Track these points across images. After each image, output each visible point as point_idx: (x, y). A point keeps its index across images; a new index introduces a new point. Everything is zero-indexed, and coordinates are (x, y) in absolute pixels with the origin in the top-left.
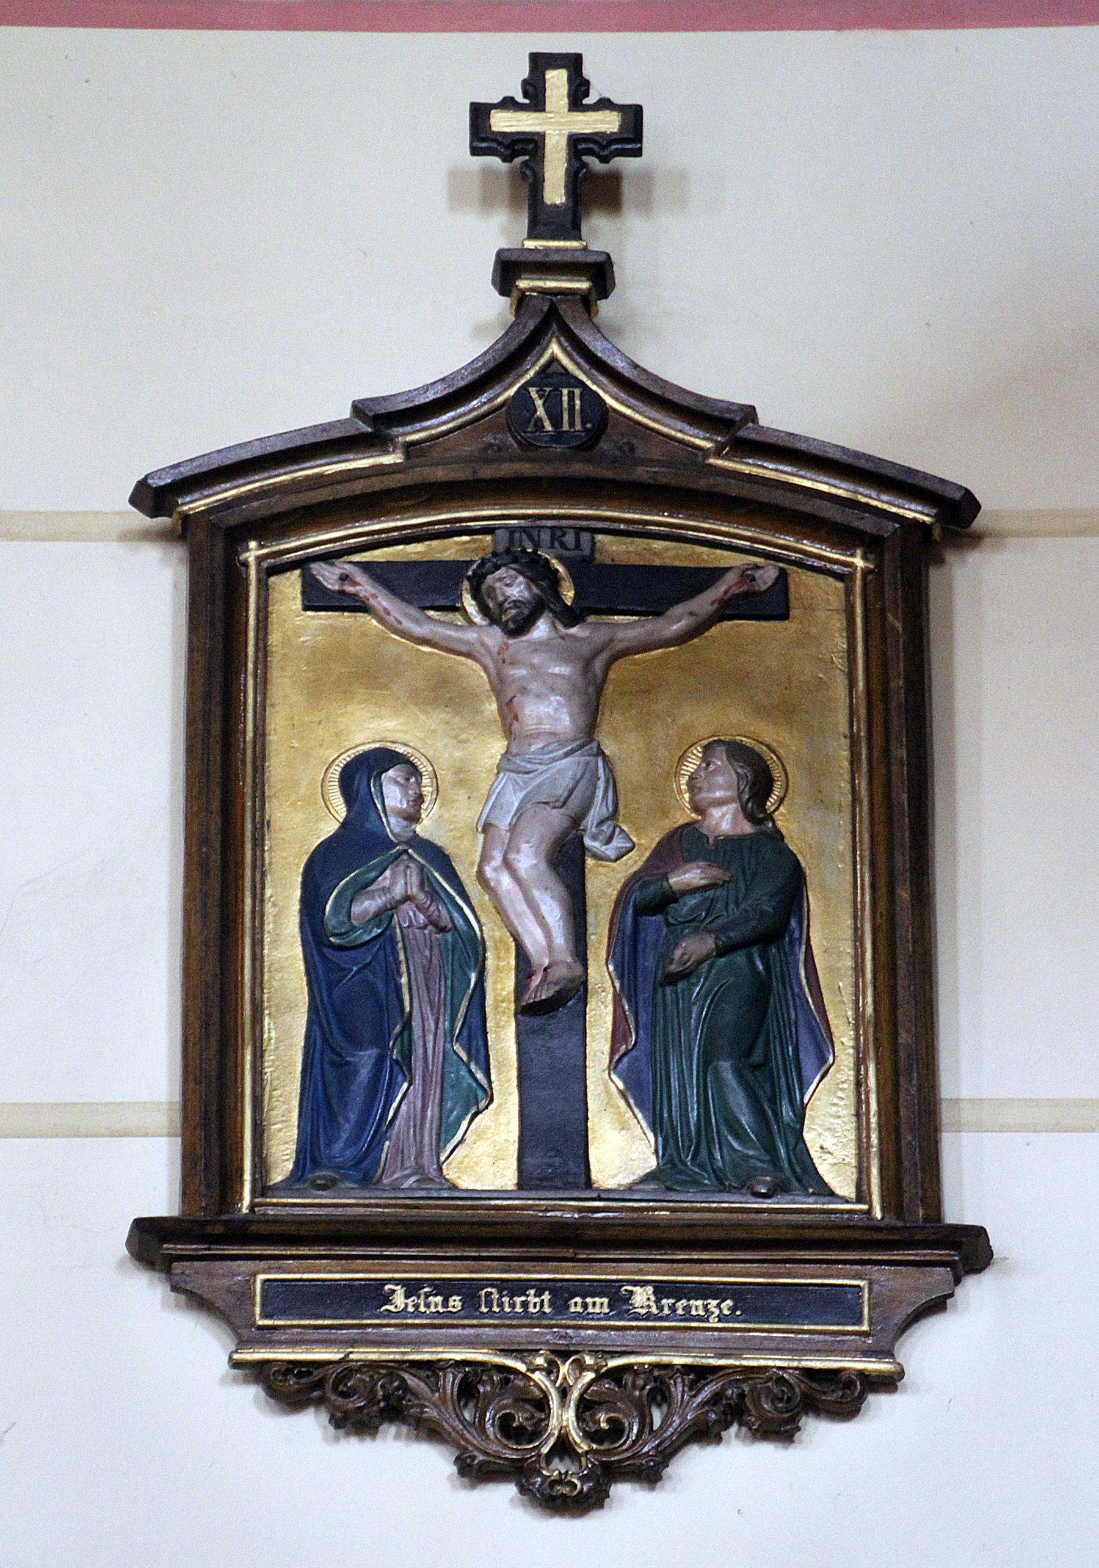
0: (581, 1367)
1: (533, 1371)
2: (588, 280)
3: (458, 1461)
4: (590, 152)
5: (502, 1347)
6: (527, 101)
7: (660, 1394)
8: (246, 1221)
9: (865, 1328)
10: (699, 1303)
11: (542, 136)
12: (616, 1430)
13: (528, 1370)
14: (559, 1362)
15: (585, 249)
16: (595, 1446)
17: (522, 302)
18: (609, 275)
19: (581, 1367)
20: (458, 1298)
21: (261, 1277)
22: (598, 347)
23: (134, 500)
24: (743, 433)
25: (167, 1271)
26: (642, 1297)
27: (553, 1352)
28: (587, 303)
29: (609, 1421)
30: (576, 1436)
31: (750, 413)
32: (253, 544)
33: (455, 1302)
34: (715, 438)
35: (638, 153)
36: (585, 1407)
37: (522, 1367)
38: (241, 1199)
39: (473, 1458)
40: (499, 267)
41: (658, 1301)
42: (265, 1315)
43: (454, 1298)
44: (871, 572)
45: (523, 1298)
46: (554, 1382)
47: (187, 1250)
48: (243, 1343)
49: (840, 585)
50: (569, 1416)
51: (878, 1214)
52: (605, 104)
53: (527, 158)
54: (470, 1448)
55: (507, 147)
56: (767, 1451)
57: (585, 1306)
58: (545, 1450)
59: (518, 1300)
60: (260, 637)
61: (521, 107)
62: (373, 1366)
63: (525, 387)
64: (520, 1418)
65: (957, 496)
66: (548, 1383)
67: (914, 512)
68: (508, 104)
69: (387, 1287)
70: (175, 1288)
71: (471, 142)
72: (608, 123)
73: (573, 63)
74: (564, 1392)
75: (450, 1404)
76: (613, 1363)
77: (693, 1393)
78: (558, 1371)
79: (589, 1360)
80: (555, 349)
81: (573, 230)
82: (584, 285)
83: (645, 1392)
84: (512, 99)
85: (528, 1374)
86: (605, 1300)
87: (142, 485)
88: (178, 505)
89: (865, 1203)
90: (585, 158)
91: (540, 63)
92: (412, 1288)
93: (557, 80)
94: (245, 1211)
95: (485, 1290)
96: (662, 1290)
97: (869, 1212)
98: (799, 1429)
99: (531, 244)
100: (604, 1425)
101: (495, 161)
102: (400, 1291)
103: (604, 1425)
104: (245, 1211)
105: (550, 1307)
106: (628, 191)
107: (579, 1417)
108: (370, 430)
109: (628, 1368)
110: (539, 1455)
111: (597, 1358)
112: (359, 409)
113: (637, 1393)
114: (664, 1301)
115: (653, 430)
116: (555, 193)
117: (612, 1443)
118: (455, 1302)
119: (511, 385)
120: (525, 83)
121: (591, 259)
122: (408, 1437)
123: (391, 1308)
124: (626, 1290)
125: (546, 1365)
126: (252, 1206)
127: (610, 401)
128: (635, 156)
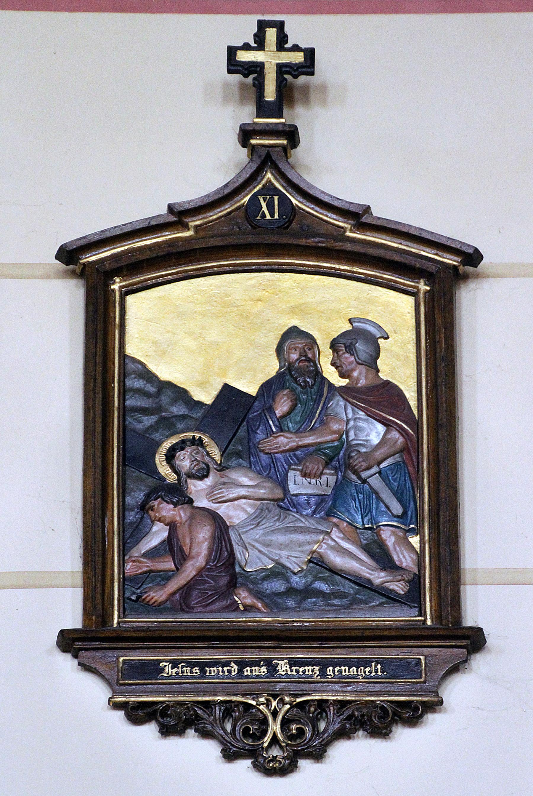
0: (282, 702)
2: (286, 139)
3: (223, 751)
8: (114, 630)
10: (215, 668)
12: (301, 732)
13: (257, 704)
17: (253, 150)
19: (282, 702)
20: (197, 668)
21: (121, 659)
22: (291, 175)
23: (57, 257)
25: (75, 656)
26: (283, 667)
27: (269, 695)
29: (297, 729)
30: (280, 736)
31: (367, 209)
32: (118, 280)
33: (196, 670)
34: (349, 221)
35: (312, 74)
36: (285, 723)
37: (254, 703)
38: (113, 619)
40: (241, 134)
41: (290, 668)
44: (428, 292)
45: (228, 668)
47: (350, 644)
48: (115, 693)
49: (410, 300)
51: (429, 622)
52: (296, 48)
55: (246, 69)
57: (251, 671)
58: (266, 745)
59: (225, 669)
60: (420, 407)
63: (255, 196)
64: (252, 728)
65: (471, 251)
66: (266, 711)
67: (450, 260)
68: (246, 47)
70: (80, 664)
71: (228, 67)
72: (298, 58)
74: (275, 714)
75: (218, 722)
76: (298, 700)
77: (338, 715)
78: (271, 704)
79: (287, 699)
80: (269, 175)
82: (285, 142)
85: (258, 707)
88: (80, 259)
89: (420, 615)
90: (286, 76)
91: (262, 26)
92: (175, 664)
93: (271, 34)
94: (115, 625)
95: (181, 664)
96: (293, 662)
99: (256, 120)
100: (294, 731)
101: (237, 78)
103: (294, 731)
104: (115, 625)
106: (313, 95)
108: (175, 219)
109: (307, 701)
110: (262, 748)
111: (291, 698)
112: (171, 208)
113: (311, 715)
114: (293, 668)
115: (310, 213)
118: (196, 670)
119: (247, 195)
120: (255, 35)
122: (198, 737)
123: (165, 675)
125: (265, 702)
126: (118, 623)
127: (294, 201)
128: (311, 75)
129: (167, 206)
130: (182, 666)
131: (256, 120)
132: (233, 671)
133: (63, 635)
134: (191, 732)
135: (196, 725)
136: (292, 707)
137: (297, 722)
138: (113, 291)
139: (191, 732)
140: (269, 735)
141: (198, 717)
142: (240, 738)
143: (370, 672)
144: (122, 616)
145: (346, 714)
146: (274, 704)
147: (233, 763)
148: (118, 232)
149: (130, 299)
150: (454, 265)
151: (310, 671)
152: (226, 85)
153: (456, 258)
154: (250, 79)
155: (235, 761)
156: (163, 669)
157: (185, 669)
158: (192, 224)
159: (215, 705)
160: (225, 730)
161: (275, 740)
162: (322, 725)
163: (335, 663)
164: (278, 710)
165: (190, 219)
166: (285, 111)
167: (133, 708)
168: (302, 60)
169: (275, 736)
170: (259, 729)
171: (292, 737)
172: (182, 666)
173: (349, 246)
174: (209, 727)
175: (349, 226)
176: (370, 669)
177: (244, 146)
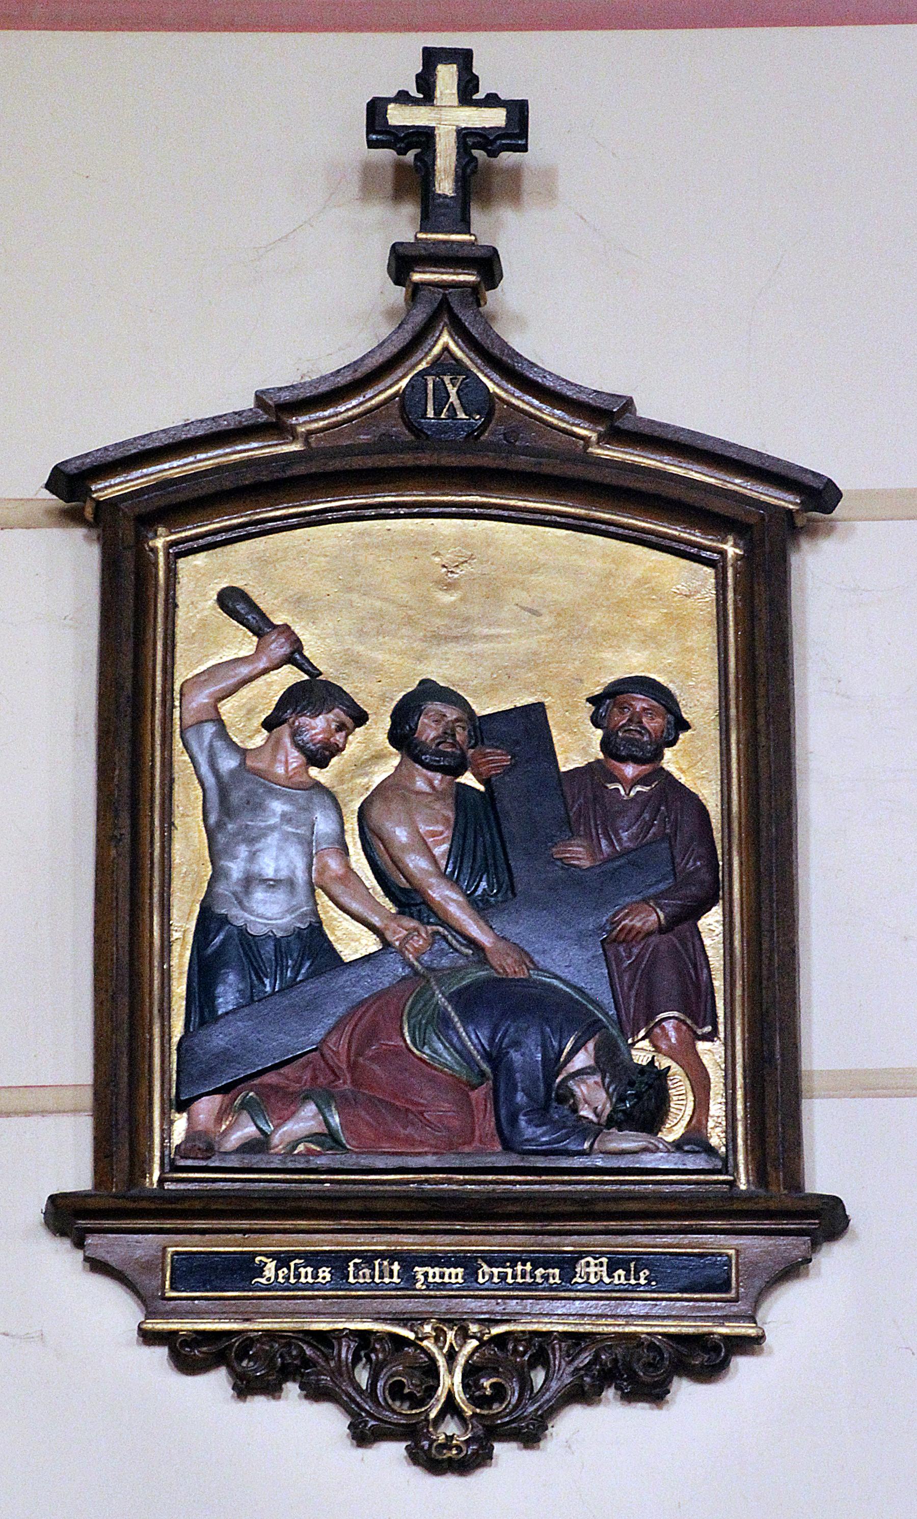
0: (464, 1335)
1: (422, 1340)
2: (479, 274)
4: (476, 146)
5: (377, 1316)
6: (421, 96)
7: (541, 1358)
9: (733, 1294)
11: (433, 128)
12: (499, 1392)
13: (417, 1338)
14: (445, 1329)
15: (472, 244)
16: (478, 1411)
17: (416, 290)
18: (495, 268)
19: (464, 1335)
20: (328, 1270)
24: (625, 424)
25: (79, 1244)
28: (475, 295)
30: (460, 1397)
32: (161, 530)
33: (325, 1274)
35: (524, 148)
36: (471, 1373)
37: (412, 1336)
39: (366, 1422)
42: (173, 1288)
43: (324, 1269)
46: (441, 1348)
48: (150, 1315)
49: (710, 571)
50: (445, 1380)
52: (492, 101)
53: (419, 150)
54: (363, 1414)
56: (641, 1411)
58: (432, 1415)
61: (416, 102)
62: (270, 1335)
65: (817, 484)
67: (788, 501)
68: (403, 98)
69: (258, 1259)
70: (87, 1259)
72: (496, 118)
73: (464, 58)
74: (451, 1357)
80: (445, 338)
81: (465, 225)
83: (526, 1358)
84: (407, 92)
86: (557, 1271)
87: (57, 471)
91: (431, 57)
92: (283, 1260)
97: (732, 1184)
98: (669, 1392)
99: (420, 236)
100: (488, 1392)
101: (386, 155)
102: (271, 1265)
105: (399, 1277)
106: (528, 183)
107: (466, 1386)
112: (260, 398)
116: (445, 185)
117: (501, 1403)
118: (325, 1274)
120: (418, 76)
121: (478, 254)
123: (263, 1281)
124: (261, 1261)
126: (161, 1181)
127: (492, 387)
129: (253, 395)
130: (355, 1264)
131: (420, 236)
132: (460, 1276)
133: (52, 1202)
134: (292, 1389)
135: (302, 1375)
136: (482, 1343)
137: (495, 1372)
138: (154, 550)
139: (292, 1389)
140: (442, 1392)
141: (307, 1362)
142: (385, 1399)
143: (287, 1278)
144: (167, 1168)
145: (585, 1358)
146: (451, 1335)
147: (371, 1448)
148: (683, 439)
149: (182, 563)
150: (790, 510)
151: (453, 1276)
152: (368, 173)
153: (791, 498)
154: (410, 156)
155: (376, 1445)
156: (260, 1271)
157: (302, 1270)
158: (301, 429)
159: (339, 1339)
160: (357, 1387)
161: (451, 1407)
162: (538, 1377)
163: (433, 1260)
164: (457, 1349)
165: (302, 419)
166: (476, 216)
167: (185, 1343)
168: (502, 123)
169: (450, 1395)
170: (420, 1386)
171: (478, 1401)
172: (355, 1264)
173: (592, 474)
174: (326, 1379)
175: (594, 436)
176: (286, 1271)
177: (397, 282)
